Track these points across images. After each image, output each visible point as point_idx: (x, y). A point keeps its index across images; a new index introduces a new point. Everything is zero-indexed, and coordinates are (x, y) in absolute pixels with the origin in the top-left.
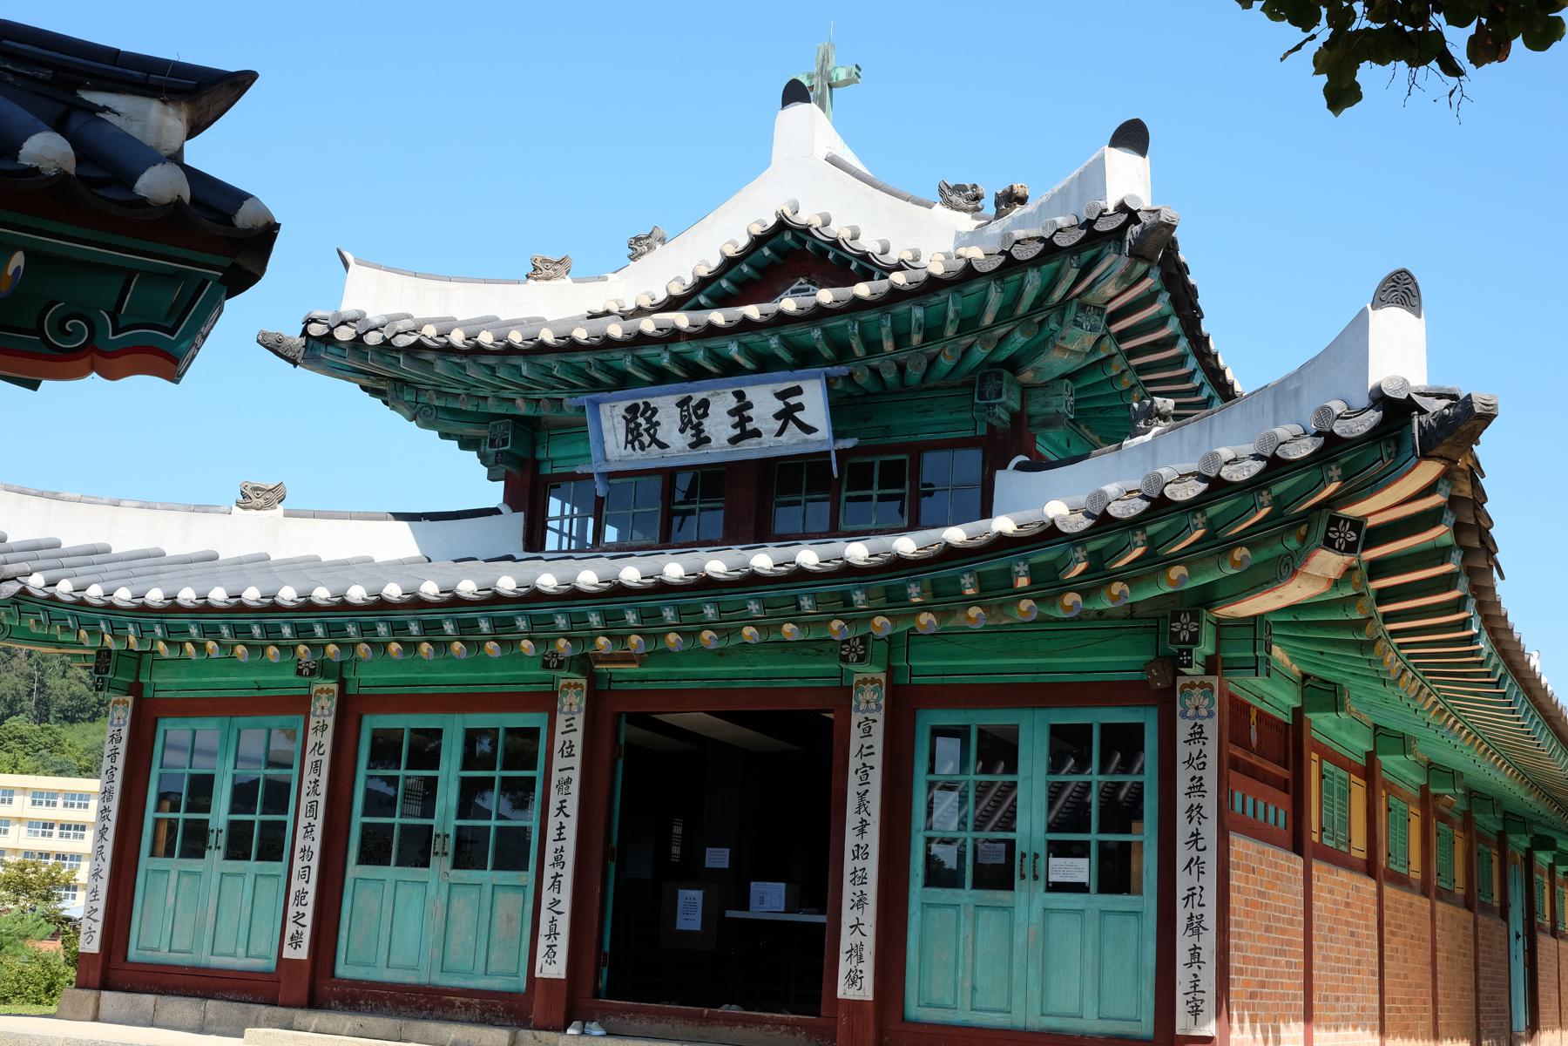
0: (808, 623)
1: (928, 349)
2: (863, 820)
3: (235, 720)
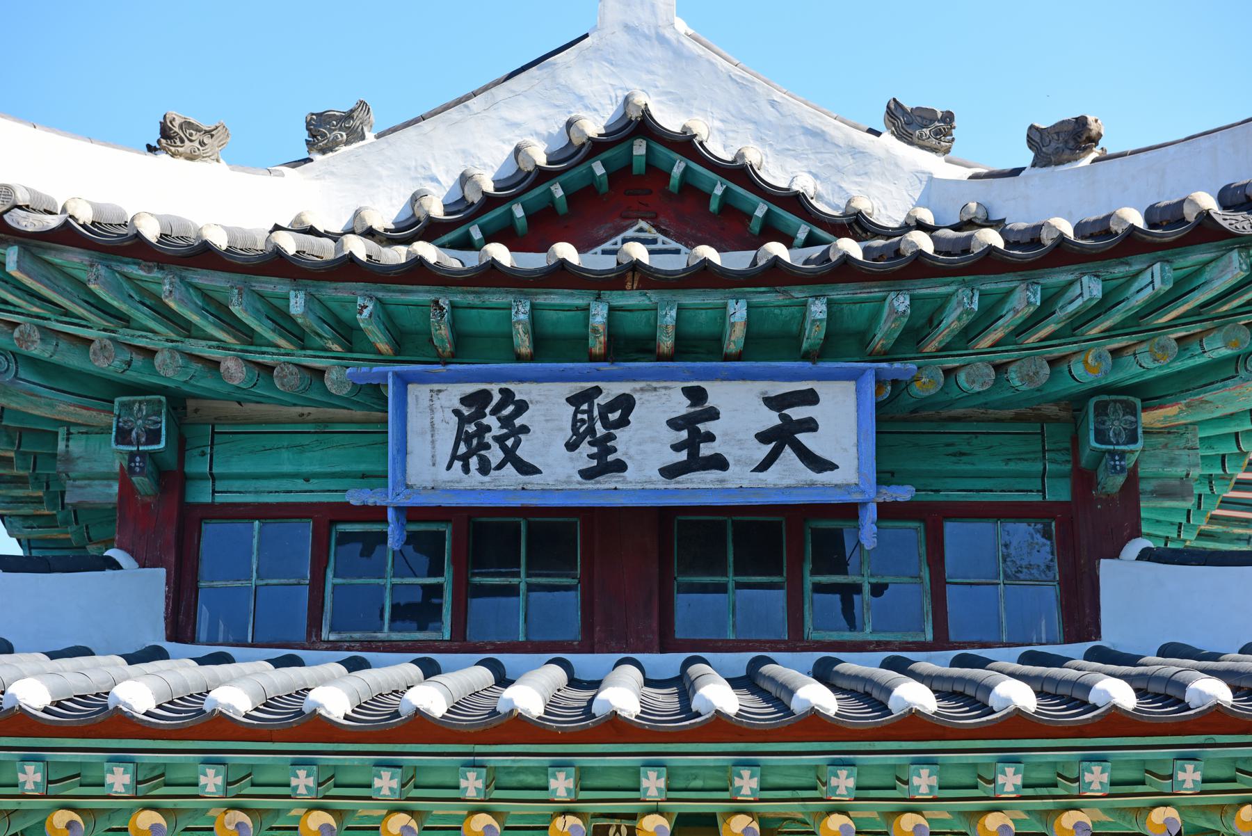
1: (1049, 352)
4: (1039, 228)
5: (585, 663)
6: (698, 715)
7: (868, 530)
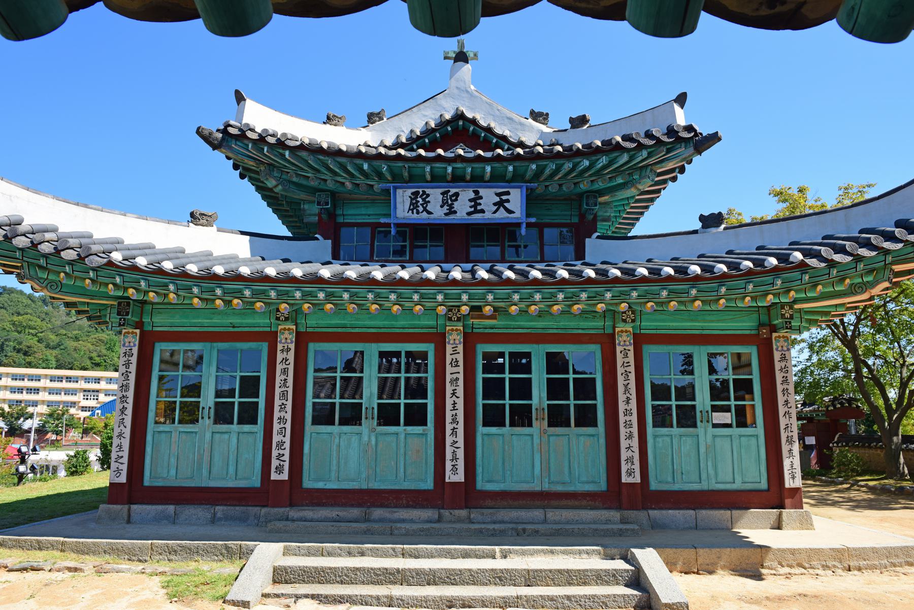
0: (248, 302)
2: (628, 398)
3: (215, 344)
4: (572, 146)
5: (446, 266)
6: (477, 279)
7: (523, 230)
